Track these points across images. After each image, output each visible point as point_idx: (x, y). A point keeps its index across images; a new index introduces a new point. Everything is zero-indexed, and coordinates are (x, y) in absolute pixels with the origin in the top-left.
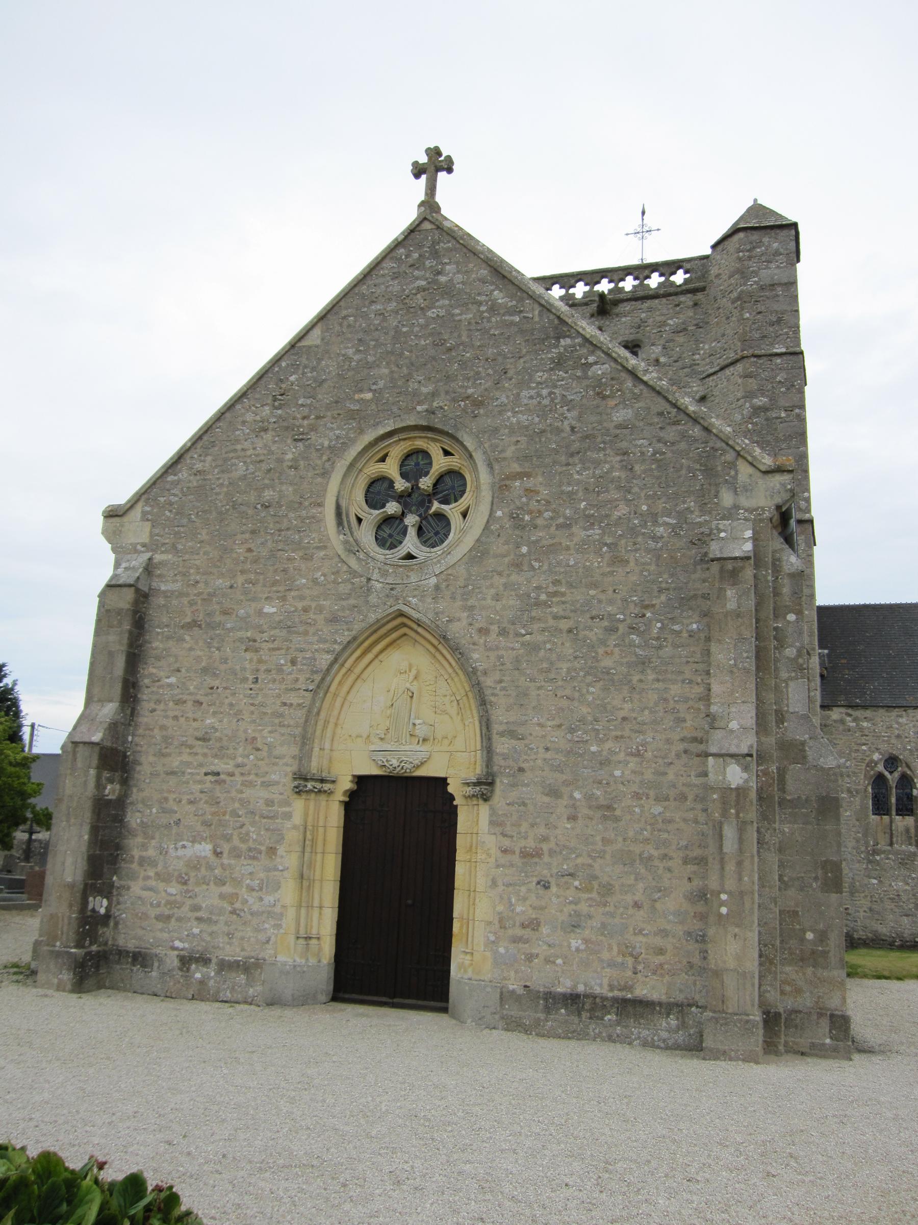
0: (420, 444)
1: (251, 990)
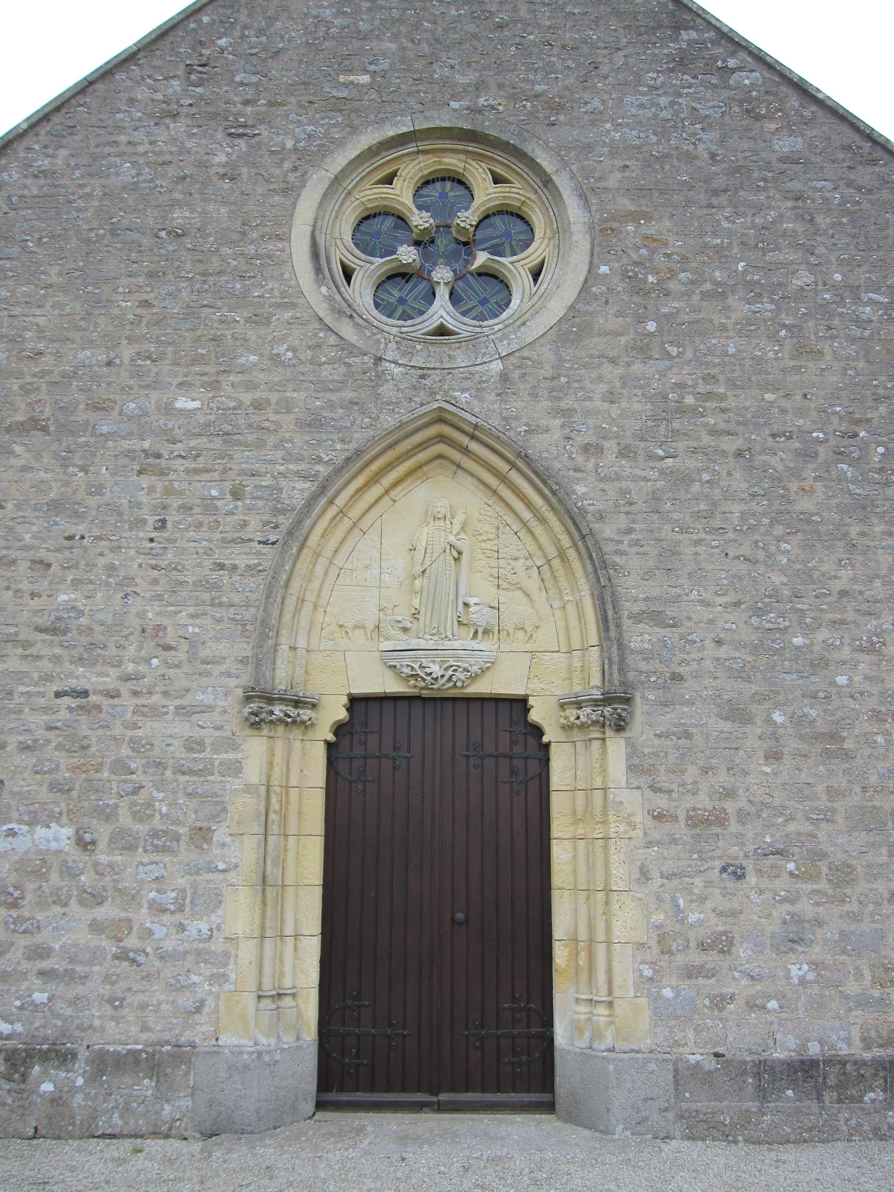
0: (453, 162)
1: (167, 1107)
